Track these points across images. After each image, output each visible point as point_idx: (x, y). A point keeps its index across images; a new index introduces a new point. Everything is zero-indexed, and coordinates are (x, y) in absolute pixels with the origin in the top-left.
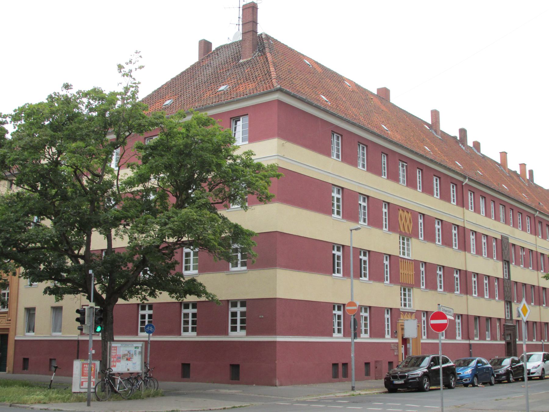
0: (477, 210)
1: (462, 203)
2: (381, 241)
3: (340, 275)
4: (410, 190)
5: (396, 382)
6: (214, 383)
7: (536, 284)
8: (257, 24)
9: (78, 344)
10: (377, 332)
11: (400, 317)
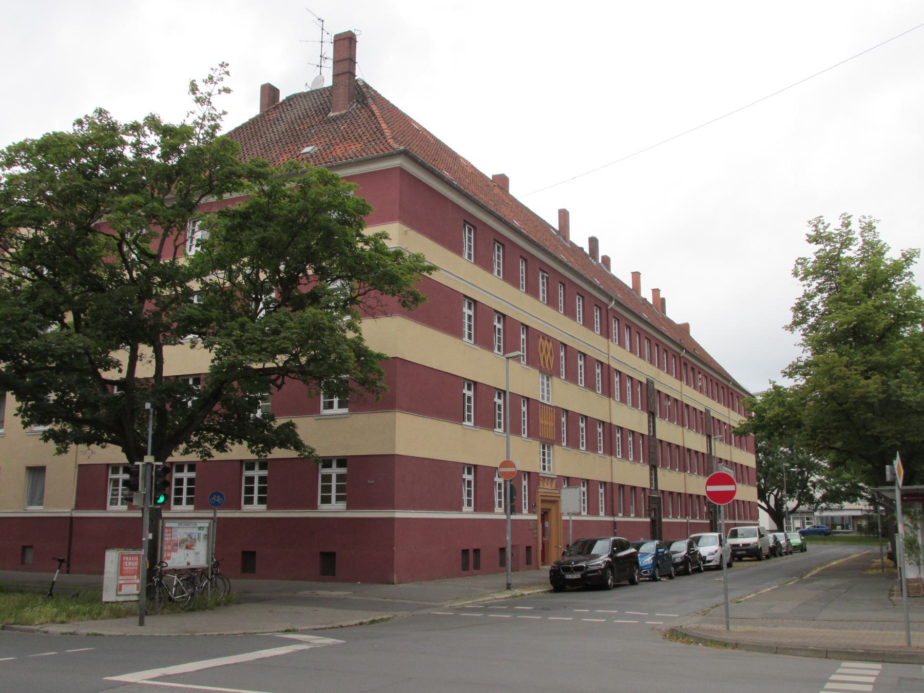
0: (621, 344)
1: (606, 333)
2: (524, 380)
3: (471, 424)
4: (549, 310)
5: (569, 576)
6: (294, 580)
7: (681, 444)
8: (355, 63)
9: (71, 524)
10: (483, 504)
11: (539, 484)
